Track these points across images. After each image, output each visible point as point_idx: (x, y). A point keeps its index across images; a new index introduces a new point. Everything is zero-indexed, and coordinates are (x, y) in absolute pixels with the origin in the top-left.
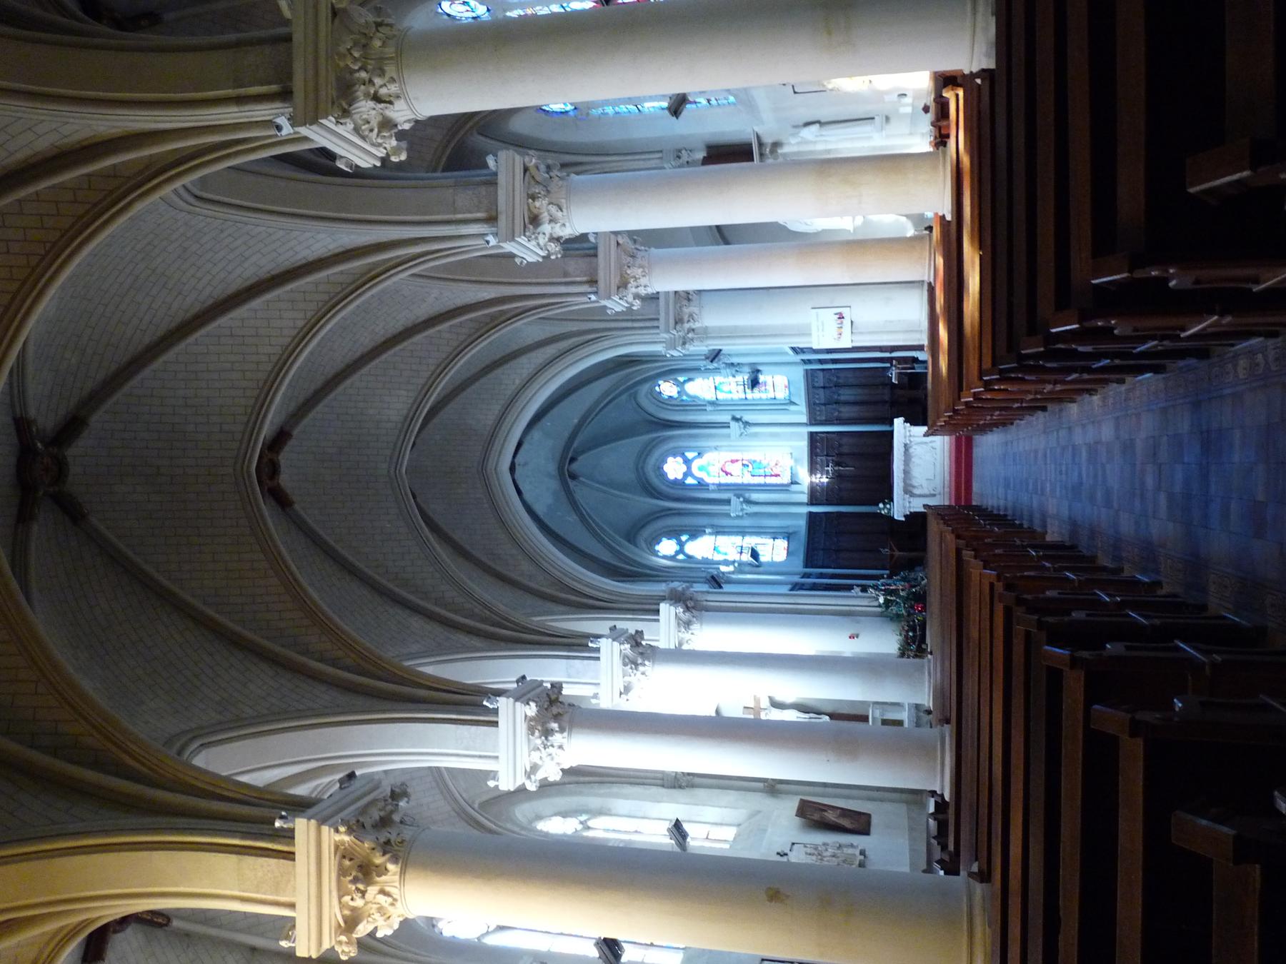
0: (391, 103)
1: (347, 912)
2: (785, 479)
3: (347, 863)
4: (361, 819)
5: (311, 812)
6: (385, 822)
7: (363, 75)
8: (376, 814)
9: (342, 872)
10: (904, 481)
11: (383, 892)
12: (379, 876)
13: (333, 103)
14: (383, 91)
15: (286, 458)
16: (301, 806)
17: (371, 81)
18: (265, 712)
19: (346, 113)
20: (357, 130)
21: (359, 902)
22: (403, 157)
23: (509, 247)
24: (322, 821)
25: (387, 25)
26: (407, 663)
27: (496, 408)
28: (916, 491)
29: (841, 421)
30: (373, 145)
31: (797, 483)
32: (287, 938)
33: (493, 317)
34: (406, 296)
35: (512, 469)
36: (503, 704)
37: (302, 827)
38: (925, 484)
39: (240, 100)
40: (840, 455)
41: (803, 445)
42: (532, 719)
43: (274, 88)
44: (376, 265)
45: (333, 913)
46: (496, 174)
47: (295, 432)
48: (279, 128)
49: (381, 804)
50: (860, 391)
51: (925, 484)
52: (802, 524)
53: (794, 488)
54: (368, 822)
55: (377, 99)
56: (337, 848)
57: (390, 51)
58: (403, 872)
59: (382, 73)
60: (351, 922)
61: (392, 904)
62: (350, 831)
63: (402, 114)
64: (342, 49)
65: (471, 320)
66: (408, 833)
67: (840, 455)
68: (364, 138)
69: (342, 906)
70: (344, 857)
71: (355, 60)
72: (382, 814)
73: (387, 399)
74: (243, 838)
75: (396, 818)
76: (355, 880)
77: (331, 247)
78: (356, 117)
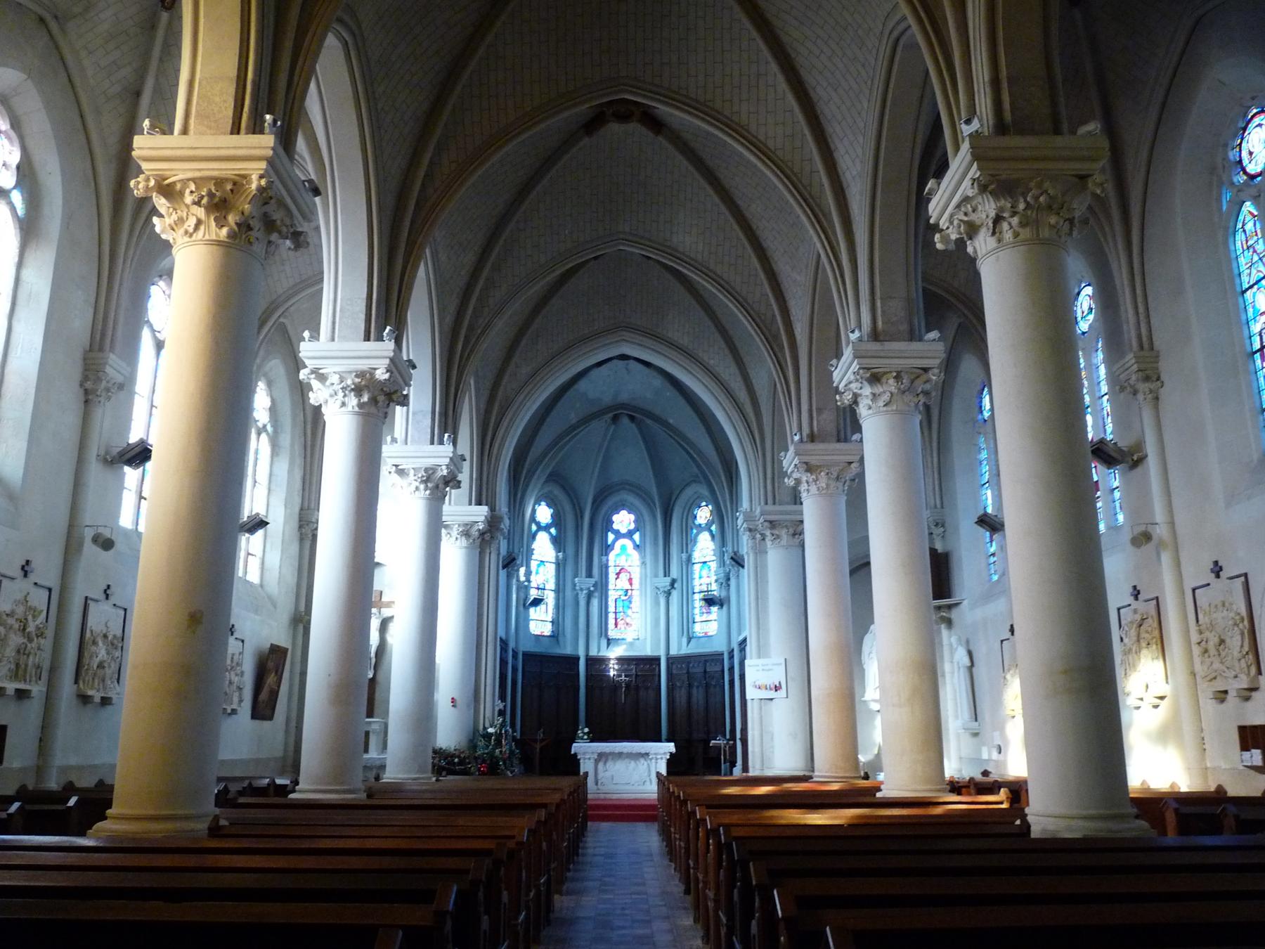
0: (994, 233)
1: (178, 186)
3: (229, 187)
4: (273, 201)
5: (281, 151)
6: (270, 225)
7: (1022, 206)
8: (277, 216)
9: (219, 182)
11: (199, 222)
12: (215, 220)
13: (992, 175)
14: (1005, 226)
15: (635, 129)
16: (286, 141)
17: (1014, 214)
18: (380, 106)
19: (983, 189)
20: (966, 199)
21: (188, 199)
22: (939, 246)
23: (848, 353)
24: (270, 161)
25: (1071, 230)
26: (428, 251)
27: (685, 341)
28: (601, 765)
29: (671, 690)
30: (952, 216)
31: (608, 644)
32: (153, 127)
33: (776, 337)
34: (798, 249)
35: (623, 357)
36: (388, 346)
37: (266, 141)
38: (608, 774)
39: (995, 83)
40: (637, 688)
41: (648, 651)
42: (372, 375)
43: (1008, 116)
44: (827, 216)
45: (179, 173)
46: (921, 340)
47: (660, 138)
48: (968, 122)
49: (288, 222)
51: (608, 774)
52: (568, 650)
53: (604, 642)
54: (271, 208)
55: (998, 220)
56: (244, 177)
57: (1045, 233)
58: (219, 243)
59: (1022, 224)
60: (168, 191)
61: (186, 232)
62: (261, 190)
63: (982, 245)
64: (1047, 185)
65: (774, 316)
66: (258, 248)
67: (637, 688)
68: (958, 206)
69: (185, 182)
70: (235, 184)
71: (1036, 198)
72: (278, 222)
73: (694, 232)
74: (254, 82)
75: (274, 237)
76: (211, 195)
77: (848, 175)
78: (980, 199)
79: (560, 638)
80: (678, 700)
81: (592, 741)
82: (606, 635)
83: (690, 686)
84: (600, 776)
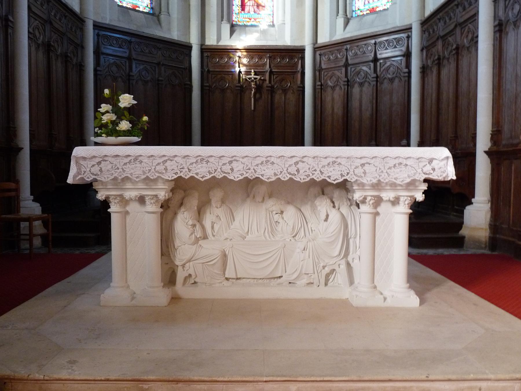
2: (238, 17)
10: (215, 183)
28: (183, 224)
29: (319, 89)
31: (232, 32)
38: (210, 249)
40: (272, 90)
41: (286, 39)
50: (367, 114)
51: (210, 249)
52: (175, 35)
53: (226, 28)
67: (272, 90)
79: (162, 17)
80: (328, 106)
81: (150, 138)
82: (229, 19)
83: (349, 84)
84: (179, 258)
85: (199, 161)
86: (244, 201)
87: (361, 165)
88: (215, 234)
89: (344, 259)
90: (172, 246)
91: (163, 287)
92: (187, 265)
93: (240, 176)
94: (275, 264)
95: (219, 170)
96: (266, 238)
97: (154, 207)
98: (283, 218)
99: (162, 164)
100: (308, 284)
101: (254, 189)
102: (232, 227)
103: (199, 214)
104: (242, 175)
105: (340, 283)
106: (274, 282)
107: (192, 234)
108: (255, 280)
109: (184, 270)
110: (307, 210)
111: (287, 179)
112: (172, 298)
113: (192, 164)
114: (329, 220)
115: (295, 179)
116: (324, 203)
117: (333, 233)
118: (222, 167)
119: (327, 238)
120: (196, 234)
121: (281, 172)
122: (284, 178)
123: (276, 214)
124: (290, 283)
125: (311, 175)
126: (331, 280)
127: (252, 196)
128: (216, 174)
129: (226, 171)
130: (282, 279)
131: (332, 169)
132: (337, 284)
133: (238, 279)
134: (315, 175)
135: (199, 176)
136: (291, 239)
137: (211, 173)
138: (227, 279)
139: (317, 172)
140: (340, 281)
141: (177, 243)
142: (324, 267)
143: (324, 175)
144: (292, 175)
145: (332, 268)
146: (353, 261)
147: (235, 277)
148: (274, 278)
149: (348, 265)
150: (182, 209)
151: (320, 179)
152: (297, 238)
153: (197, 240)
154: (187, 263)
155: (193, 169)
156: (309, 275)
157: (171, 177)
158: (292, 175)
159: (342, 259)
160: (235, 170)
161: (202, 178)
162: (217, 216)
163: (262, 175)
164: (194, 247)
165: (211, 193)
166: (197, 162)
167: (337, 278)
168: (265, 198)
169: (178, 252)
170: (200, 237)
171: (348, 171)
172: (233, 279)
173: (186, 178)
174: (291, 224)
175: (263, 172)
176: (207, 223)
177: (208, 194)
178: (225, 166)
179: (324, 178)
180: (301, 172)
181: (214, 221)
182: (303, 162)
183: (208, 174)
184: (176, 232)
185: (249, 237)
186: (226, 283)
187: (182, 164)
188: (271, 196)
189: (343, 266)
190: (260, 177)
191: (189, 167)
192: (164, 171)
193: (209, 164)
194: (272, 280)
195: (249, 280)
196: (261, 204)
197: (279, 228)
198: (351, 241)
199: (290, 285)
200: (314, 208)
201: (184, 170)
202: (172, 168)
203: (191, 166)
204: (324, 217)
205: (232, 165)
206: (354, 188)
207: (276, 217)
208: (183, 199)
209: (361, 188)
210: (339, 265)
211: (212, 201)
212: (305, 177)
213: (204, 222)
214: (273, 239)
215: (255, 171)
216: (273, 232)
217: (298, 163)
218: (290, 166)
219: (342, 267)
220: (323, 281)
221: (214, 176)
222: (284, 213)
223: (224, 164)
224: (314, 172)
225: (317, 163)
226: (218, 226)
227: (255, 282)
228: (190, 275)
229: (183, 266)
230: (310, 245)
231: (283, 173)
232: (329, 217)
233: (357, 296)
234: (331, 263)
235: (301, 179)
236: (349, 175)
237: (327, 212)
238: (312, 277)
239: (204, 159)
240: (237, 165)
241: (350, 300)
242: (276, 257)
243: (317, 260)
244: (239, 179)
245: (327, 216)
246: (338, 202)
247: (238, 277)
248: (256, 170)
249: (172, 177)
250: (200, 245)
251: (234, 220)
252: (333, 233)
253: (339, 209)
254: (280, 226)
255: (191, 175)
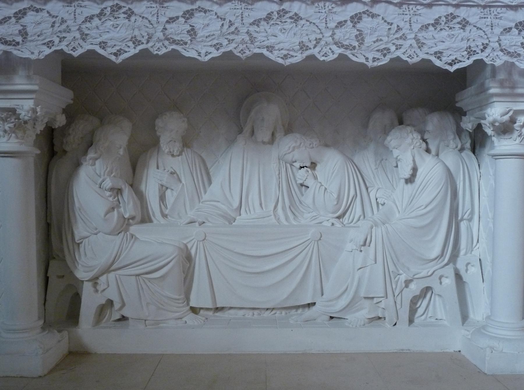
28: (91, 187)
51: (154, 243)
85: (108, 11)
86: (231, 142)
87: (516, 25)
88: (167, 212)
89: (451, 265)
90: (69, 237)
91: (43, 328)
92: (103, 279)
93: (212, 49)
94: (304, 268)
95: (160, 35)
96: (278, 220)
97: (13, 140)
98: (316, 178)
99: (13, 20)
100: (372, 320)
101: (252, 114)
102: (205, 197)
103: (134, 168)
104: (217, 47)
105: (439, 317)
106: (295, 316)
107: (113, 209)
108: (256, 312)
109: (97, 291)
110: (367, 161)
111: (331, 57)
112: (70, 353)
113: (89, 19)
114: (419, 179)
115: (354, 59)
116: (409, 140)
117: (428, 209)
118: (168, 26)
119: (416, 217)
120: (122, 210)
121: (318, 41)
122: (325, 55)
123: (301, 167)
124: (332, 318)
125: (393, 48)
126: (420, 311)
127: (247, 129)
128: (150, 44)
129: (177, 38)
130: (314, 308)
131: (444, 33)
132: (433, 320)
133: (217, 309)
134: (402, 50)
135: (110, 50)
136: (335, 221)
137: (140, 43)
138: (194, 310)
139: (409, 42)
140: (441, 314)
141: (80, 230)
142: (407, 283)
143: (425, 49)
144: (347, 47)
145: (424, 284)
146: (467, 270)
147: (210, 306)
148: (297, 307)
149: (458, 277)
150: (91, 155)
151: (416, 60)
152: (346, 220)
153: (125, 224)
154: (103, 274)
155: (93, 33)
156: (375, 300)
157: (36, 52)
158: (347, 47)
159: (446, 265)
160: (201, 33)
161: (115, 54)
162: (172, 173)
163: (270, 48)
164: (118, 239)
165: (159, 123)
166: (101, 14)
167: (434, 305)
168: (277, 135)
169: (82, 249)
170: (133, 218)
171: (486, 41)
172: (208, 309)
173: (76, 54)
174: (333, 188)
175: (273, 40)
176: (151, 188)
177: (153, 127)
178: (173, 25)
179: (426, 57)
180: (369, 40)
181: (164, 183)
182: (373, 16)
183: (130, 44)
184: (77, 205)
185: (242, 219)
186: (190, 318)
187: (63, 21)
188: (289, 130)
189: (449, 281)
190: (265, 52)
191: (83, 26)
192: (19, 39)
193: (133, 18)
194: (293, 312)
195: (242, 312)
196: (268, 146)
197: (308, 199)
198: (463, 226)
199: (333, 321)
200: (383, 154)
201: (69, 37)
202: (38, 30)
203: (88, 25)
204: (407, 173)
205: (193, 21)
206: (492, 91)
207: (302, 175)
208: (92, 133)
209: (507, 91)
210: (440, 278)
211: (162, 141)
212: (378, 55)
213: (143, 187)
214: (294, 223)
215: (252, 40)
216: (294, 207)
217: (360, 18)
218: (341, 24)
219: (445, 281)
220: (404, 314)
221: (146, 50)
222: (318, 167)
223: (172, 20)
224: (400, 42)
225: (407, 18)
226: (175, 194)
227: (256, 316)
228: (110, 303)
229: (95, 280)
230: (378, 233)
231: (323, 43)
232: (418, 173)
233: (492, 348)
234: (424, 273)
235: (367, 59)
236: (488, 50)
237: (414, 161)
238: (382, 305)
239: (120, 8)
240: (206, 22)
241: (468, 357)
242: (299, 266)
243: (392, 268)
244: (209, 57)
245: (415, 170)
246: (436, 142)
247: (219, 305)
248: (255, 35)
249: (40, 52)
250: (132, 236)
251: (210, 182)
252: (428, 209)
253: (437, 155)
254: (310, 193)
255: (87, 47)
